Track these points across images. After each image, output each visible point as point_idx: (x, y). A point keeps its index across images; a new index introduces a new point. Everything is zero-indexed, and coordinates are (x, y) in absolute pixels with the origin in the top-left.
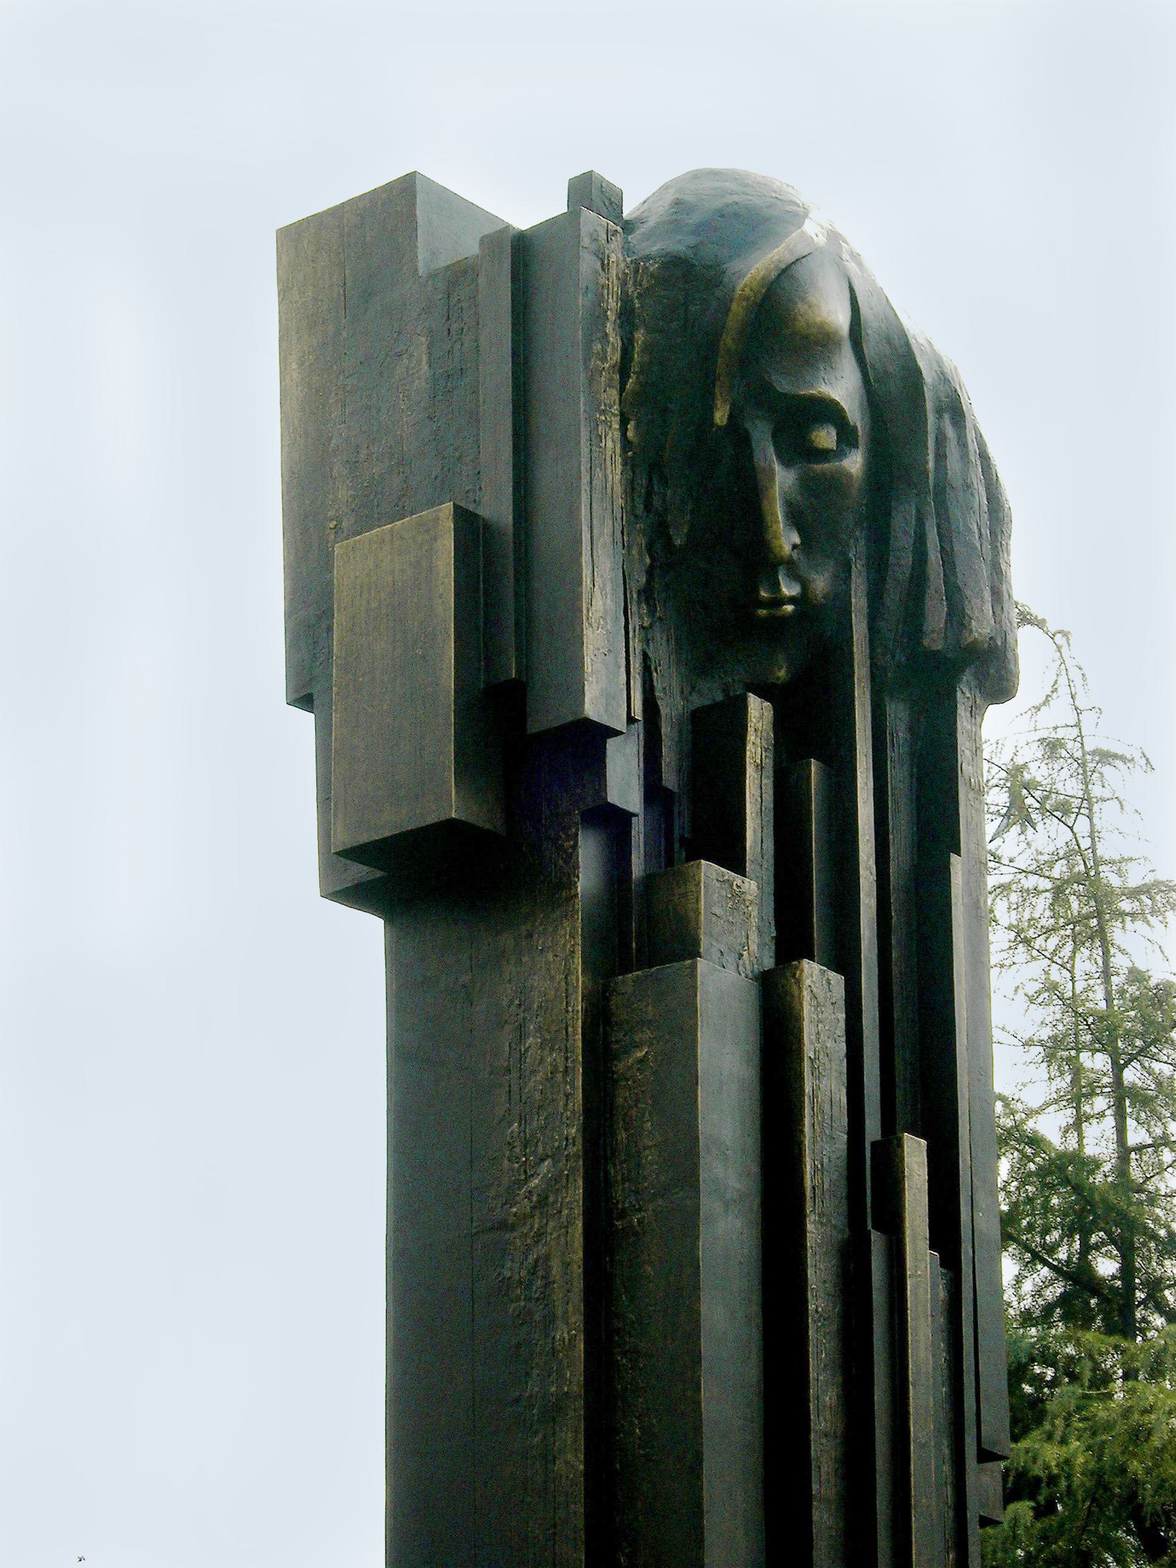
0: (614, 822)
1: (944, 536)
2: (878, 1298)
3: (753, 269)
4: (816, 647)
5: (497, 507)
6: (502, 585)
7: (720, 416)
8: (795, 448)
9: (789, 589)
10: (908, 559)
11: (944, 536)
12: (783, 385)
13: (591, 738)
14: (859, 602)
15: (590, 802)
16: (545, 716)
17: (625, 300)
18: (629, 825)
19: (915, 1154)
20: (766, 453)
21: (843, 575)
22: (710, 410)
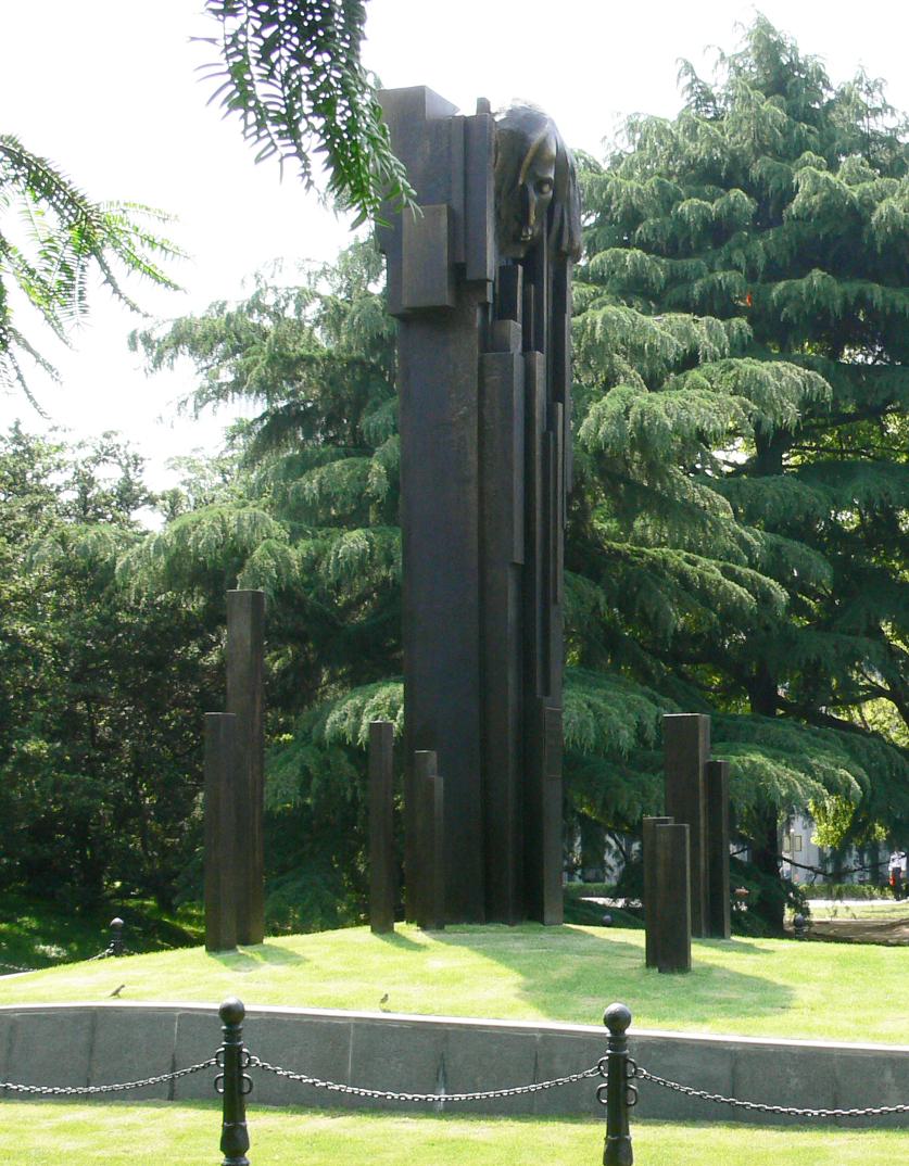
0: (485, 306)
1: (569, 213)
2: (551, 491)
3: (537, 137)
4: (534, 249)
5: (457, 204)
6: (461, 230)
7: (521, 182)
8: (539, 190)
9: (530, 232)
10: (560, 212)
11: (569, 220)
12: (539, 173)
13: (482, 283)
14: (545, 234)
15: (482, 301)
16: (471, 275)
17: (497, 142)
18: (565, 564)
19: (552, 435)
20: (531, 189)
21: (603, 720)
22: (518, 181)
